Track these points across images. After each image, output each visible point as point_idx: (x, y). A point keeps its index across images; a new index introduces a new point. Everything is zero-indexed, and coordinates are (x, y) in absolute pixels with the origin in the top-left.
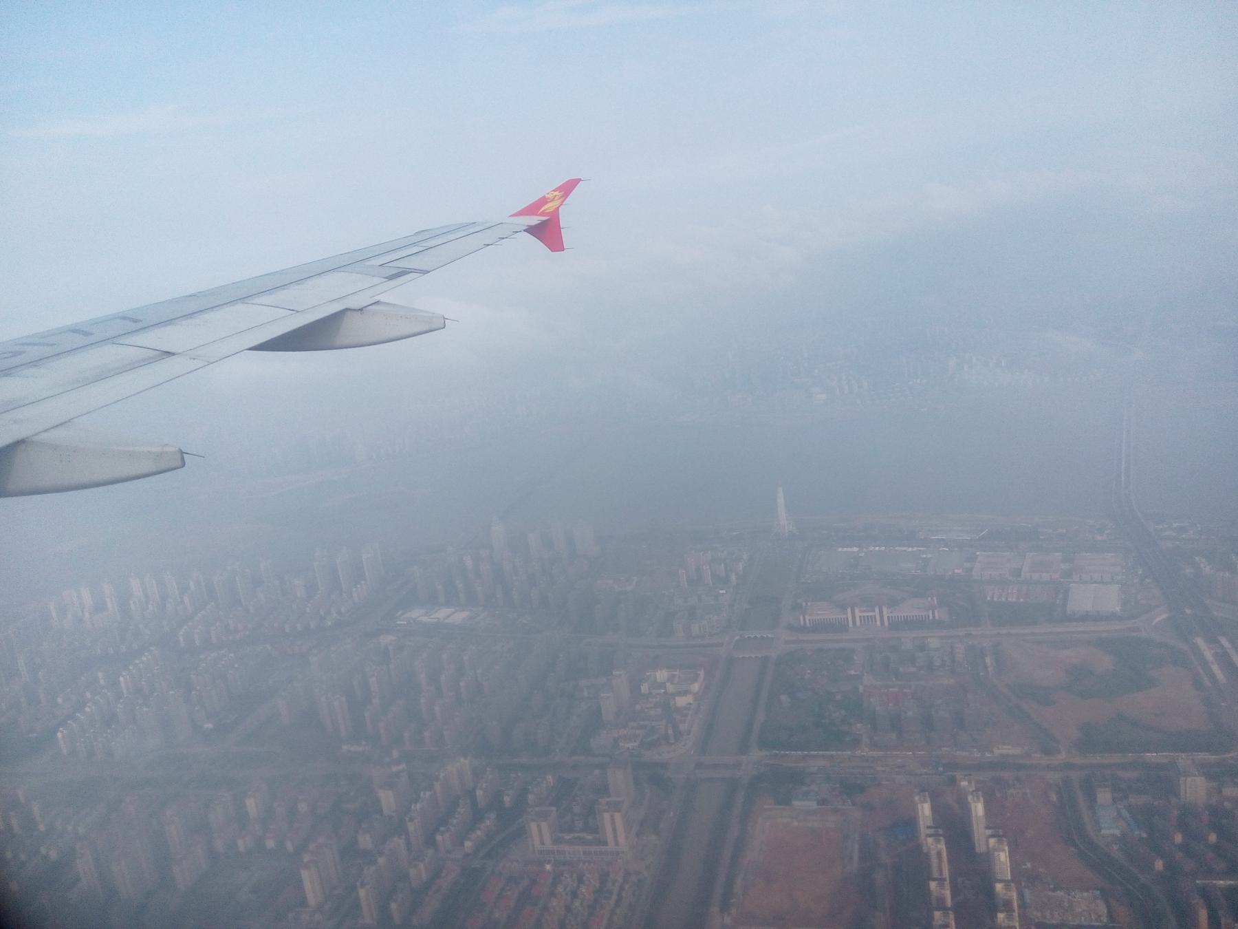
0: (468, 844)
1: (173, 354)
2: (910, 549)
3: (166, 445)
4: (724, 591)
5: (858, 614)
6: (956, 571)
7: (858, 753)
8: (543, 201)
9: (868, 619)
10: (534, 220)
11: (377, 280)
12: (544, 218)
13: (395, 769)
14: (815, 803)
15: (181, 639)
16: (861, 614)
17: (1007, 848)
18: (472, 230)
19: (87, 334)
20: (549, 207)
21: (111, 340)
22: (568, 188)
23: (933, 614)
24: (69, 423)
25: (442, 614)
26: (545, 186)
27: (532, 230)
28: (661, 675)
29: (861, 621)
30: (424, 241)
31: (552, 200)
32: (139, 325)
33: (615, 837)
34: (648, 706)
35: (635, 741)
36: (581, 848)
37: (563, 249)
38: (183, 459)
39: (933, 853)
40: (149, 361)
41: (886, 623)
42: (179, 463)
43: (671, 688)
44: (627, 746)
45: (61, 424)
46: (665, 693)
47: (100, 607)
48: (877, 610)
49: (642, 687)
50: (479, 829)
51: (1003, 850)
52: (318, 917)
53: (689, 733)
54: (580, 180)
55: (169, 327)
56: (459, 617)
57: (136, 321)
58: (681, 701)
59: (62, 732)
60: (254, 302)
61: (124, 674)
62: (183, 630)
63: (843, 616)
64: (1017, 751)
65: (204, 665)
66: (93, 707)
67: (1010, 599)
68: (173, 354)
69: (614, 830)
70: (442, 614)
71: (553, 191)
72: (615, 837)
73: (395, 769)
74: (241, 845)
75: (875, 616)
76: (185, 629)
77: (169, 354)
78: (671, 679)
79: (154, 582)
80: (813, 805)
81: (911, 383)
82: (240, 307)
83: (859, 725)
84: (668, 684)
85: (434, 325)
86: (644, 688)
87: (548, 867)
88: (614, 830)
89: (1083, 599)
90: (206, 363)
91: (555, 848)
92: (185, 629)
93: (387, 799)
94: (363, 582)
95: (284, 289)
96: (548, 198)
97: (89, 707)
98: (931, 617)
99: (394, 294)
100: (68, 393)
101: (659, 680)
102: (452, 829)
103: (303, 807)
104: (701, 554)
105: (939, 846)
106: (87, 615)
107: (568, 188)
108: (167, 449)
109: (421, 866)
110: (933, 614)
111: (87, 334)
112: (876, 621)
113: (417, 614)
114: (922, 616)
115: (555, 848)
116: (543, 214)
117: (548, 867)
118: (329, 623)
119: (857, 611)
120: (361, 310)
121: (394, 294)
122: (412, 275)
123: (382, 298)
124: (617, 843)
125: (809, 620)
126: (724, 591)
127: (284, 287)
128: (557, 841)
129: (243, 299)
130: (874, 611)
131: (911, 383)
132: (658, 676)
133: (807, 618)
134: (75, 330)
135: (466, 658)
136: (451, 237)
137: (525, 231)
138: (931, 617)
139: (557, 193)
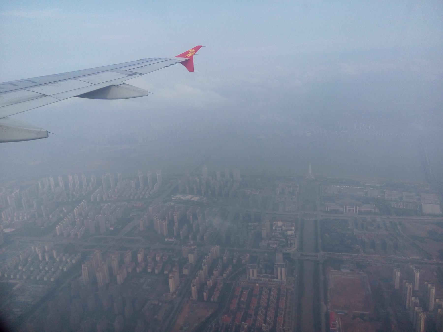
0: (225, 275)
1: (47, 96)
2: (359, 188)
3: (42, 129)
4: (294, 197)
5: (347, 208)
6: (378, 196)
7: (360, 255)
8: (188, 52)
9: (351, 210)
10: (184, 59)
11: (124, 76)
12: (188, 59)
13: (193, 247)
14: (349, 270)
15: (92, 198)
16: (349, 208)
17: (435, 288)
18: (161, 61)
19: (16, 85)
20: (189, 55)
21: (24, 88)
22: (197, 48)
23: (375, 210)
24: (6, 118)
25: (189, 197)
26: (189, 48)
27: (182, 63)
28: (280, 224)
29: (348, 210)
30: (143, 63)
31: (191, 53)
32: (35, 84)
33: (281, 276)
34: (277, 233)
35: (276, 245)
36: (268, 279)
37: (193, 71)
38: (48, 135)
39: (409, 288)
40: (38, 97)
41: (357, 212)
42: (46, 136)
43: (284, 228)
44: (273, 246)
45: (3, 118)
46: (282, 230)
47: (57, 185)
48: (355, 207)
49: (273, 227)
50: (228, 270)
51: (434, 289)
52: (174, 296)
53: (295, 244)
54: (202, 46)
55: (47, 86)
56: (196, 198)
57: (34, 82)
58: (289, 233)
59: (58, 227)
60: (78, 79)
61: (76, 208)
62: (92, 195)
63: (353, 208)
64: (418, 258)
65: (105, 208)
66: (67, 219)
67: (400, 207)
68: (47, 96)
69: (281, 274)
70: (189, 197)
71: (192, 49)
72: (281, 276)
73: (193, 247)
74: (138, 270)
75: (354, 209)
76: (99, 195)
77: (45, 95)
78: (283, 225)
79: (78, 177)
80: (348, 271)
81: (341, 132)
82: (73, 81)
83: (357, 246)
84: (283, 227)
85: (143, 94)
86: (274, 228)
87: (257, 285)
88: (281, 274)
89: (427, 208)
90: (59, 100)
91: (258, 278)
92: (99, 195)
93: (191, 258)
94: (157, 184)
95: (90, 75)
96: (190, 52)
97: (65, 219)
98: (374, 211)
99: (135, 82)
100: (7, 106)
101: (278, 225)
102: (218, 269)
103: (158, 259)
104: (283, 183)
105: (410, 286)
106: (52, 187)
107: (197, 48)
108: (42, 130)
109: (211, 281)
110: (375, 210)
111: (16, 85)
112: (354, 211)
113: (179, 196)
114: (337, 209)
115: (258, 278)
116: (187, 57)
117: (257, 285)
118: (147, 197)
119: (347, 207)
120: (117, 86)
121: (135, 82)
122: (138, 75)
123: (126, 82)
124: (281, 279)
125: (358, 210)
126: (294, 197)
127: (89, 75)
128: (258, 276)
129: (74, 78)
130: (353, 207)
131: (341, 132)
132: (278, 224)
133: (328, 208)
134: (11, 84)
135: (197, 211)
136: (153, 62)
137: (180, 63)
138: (374, 211)
139: (193, 50)
